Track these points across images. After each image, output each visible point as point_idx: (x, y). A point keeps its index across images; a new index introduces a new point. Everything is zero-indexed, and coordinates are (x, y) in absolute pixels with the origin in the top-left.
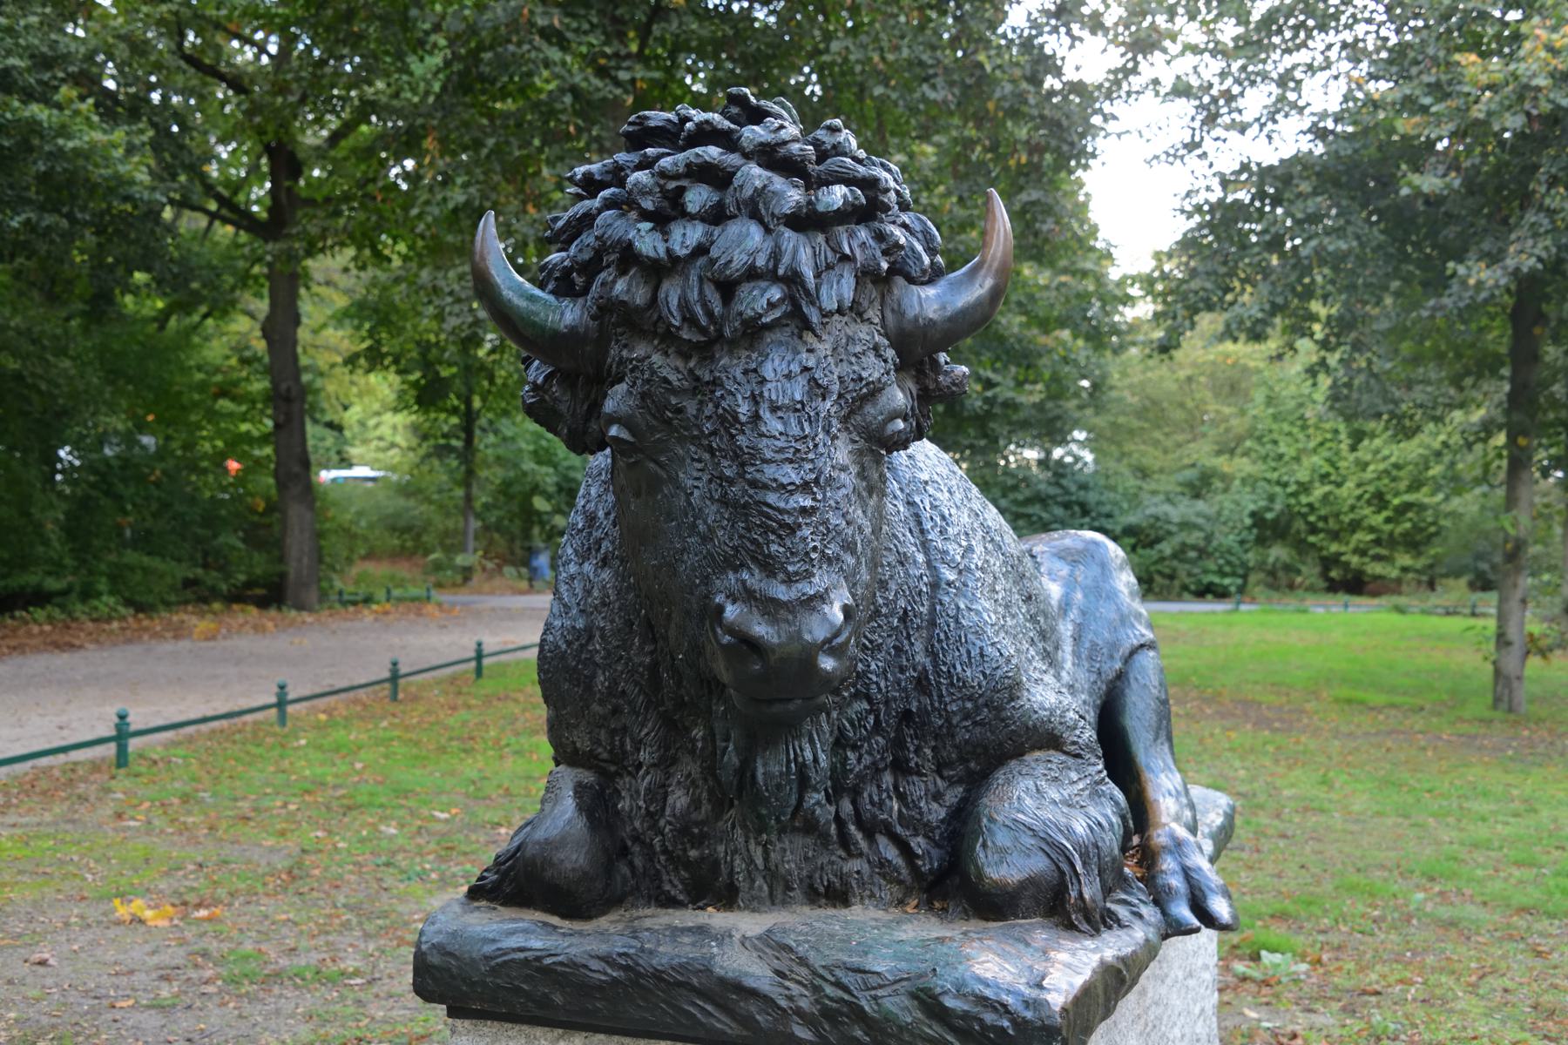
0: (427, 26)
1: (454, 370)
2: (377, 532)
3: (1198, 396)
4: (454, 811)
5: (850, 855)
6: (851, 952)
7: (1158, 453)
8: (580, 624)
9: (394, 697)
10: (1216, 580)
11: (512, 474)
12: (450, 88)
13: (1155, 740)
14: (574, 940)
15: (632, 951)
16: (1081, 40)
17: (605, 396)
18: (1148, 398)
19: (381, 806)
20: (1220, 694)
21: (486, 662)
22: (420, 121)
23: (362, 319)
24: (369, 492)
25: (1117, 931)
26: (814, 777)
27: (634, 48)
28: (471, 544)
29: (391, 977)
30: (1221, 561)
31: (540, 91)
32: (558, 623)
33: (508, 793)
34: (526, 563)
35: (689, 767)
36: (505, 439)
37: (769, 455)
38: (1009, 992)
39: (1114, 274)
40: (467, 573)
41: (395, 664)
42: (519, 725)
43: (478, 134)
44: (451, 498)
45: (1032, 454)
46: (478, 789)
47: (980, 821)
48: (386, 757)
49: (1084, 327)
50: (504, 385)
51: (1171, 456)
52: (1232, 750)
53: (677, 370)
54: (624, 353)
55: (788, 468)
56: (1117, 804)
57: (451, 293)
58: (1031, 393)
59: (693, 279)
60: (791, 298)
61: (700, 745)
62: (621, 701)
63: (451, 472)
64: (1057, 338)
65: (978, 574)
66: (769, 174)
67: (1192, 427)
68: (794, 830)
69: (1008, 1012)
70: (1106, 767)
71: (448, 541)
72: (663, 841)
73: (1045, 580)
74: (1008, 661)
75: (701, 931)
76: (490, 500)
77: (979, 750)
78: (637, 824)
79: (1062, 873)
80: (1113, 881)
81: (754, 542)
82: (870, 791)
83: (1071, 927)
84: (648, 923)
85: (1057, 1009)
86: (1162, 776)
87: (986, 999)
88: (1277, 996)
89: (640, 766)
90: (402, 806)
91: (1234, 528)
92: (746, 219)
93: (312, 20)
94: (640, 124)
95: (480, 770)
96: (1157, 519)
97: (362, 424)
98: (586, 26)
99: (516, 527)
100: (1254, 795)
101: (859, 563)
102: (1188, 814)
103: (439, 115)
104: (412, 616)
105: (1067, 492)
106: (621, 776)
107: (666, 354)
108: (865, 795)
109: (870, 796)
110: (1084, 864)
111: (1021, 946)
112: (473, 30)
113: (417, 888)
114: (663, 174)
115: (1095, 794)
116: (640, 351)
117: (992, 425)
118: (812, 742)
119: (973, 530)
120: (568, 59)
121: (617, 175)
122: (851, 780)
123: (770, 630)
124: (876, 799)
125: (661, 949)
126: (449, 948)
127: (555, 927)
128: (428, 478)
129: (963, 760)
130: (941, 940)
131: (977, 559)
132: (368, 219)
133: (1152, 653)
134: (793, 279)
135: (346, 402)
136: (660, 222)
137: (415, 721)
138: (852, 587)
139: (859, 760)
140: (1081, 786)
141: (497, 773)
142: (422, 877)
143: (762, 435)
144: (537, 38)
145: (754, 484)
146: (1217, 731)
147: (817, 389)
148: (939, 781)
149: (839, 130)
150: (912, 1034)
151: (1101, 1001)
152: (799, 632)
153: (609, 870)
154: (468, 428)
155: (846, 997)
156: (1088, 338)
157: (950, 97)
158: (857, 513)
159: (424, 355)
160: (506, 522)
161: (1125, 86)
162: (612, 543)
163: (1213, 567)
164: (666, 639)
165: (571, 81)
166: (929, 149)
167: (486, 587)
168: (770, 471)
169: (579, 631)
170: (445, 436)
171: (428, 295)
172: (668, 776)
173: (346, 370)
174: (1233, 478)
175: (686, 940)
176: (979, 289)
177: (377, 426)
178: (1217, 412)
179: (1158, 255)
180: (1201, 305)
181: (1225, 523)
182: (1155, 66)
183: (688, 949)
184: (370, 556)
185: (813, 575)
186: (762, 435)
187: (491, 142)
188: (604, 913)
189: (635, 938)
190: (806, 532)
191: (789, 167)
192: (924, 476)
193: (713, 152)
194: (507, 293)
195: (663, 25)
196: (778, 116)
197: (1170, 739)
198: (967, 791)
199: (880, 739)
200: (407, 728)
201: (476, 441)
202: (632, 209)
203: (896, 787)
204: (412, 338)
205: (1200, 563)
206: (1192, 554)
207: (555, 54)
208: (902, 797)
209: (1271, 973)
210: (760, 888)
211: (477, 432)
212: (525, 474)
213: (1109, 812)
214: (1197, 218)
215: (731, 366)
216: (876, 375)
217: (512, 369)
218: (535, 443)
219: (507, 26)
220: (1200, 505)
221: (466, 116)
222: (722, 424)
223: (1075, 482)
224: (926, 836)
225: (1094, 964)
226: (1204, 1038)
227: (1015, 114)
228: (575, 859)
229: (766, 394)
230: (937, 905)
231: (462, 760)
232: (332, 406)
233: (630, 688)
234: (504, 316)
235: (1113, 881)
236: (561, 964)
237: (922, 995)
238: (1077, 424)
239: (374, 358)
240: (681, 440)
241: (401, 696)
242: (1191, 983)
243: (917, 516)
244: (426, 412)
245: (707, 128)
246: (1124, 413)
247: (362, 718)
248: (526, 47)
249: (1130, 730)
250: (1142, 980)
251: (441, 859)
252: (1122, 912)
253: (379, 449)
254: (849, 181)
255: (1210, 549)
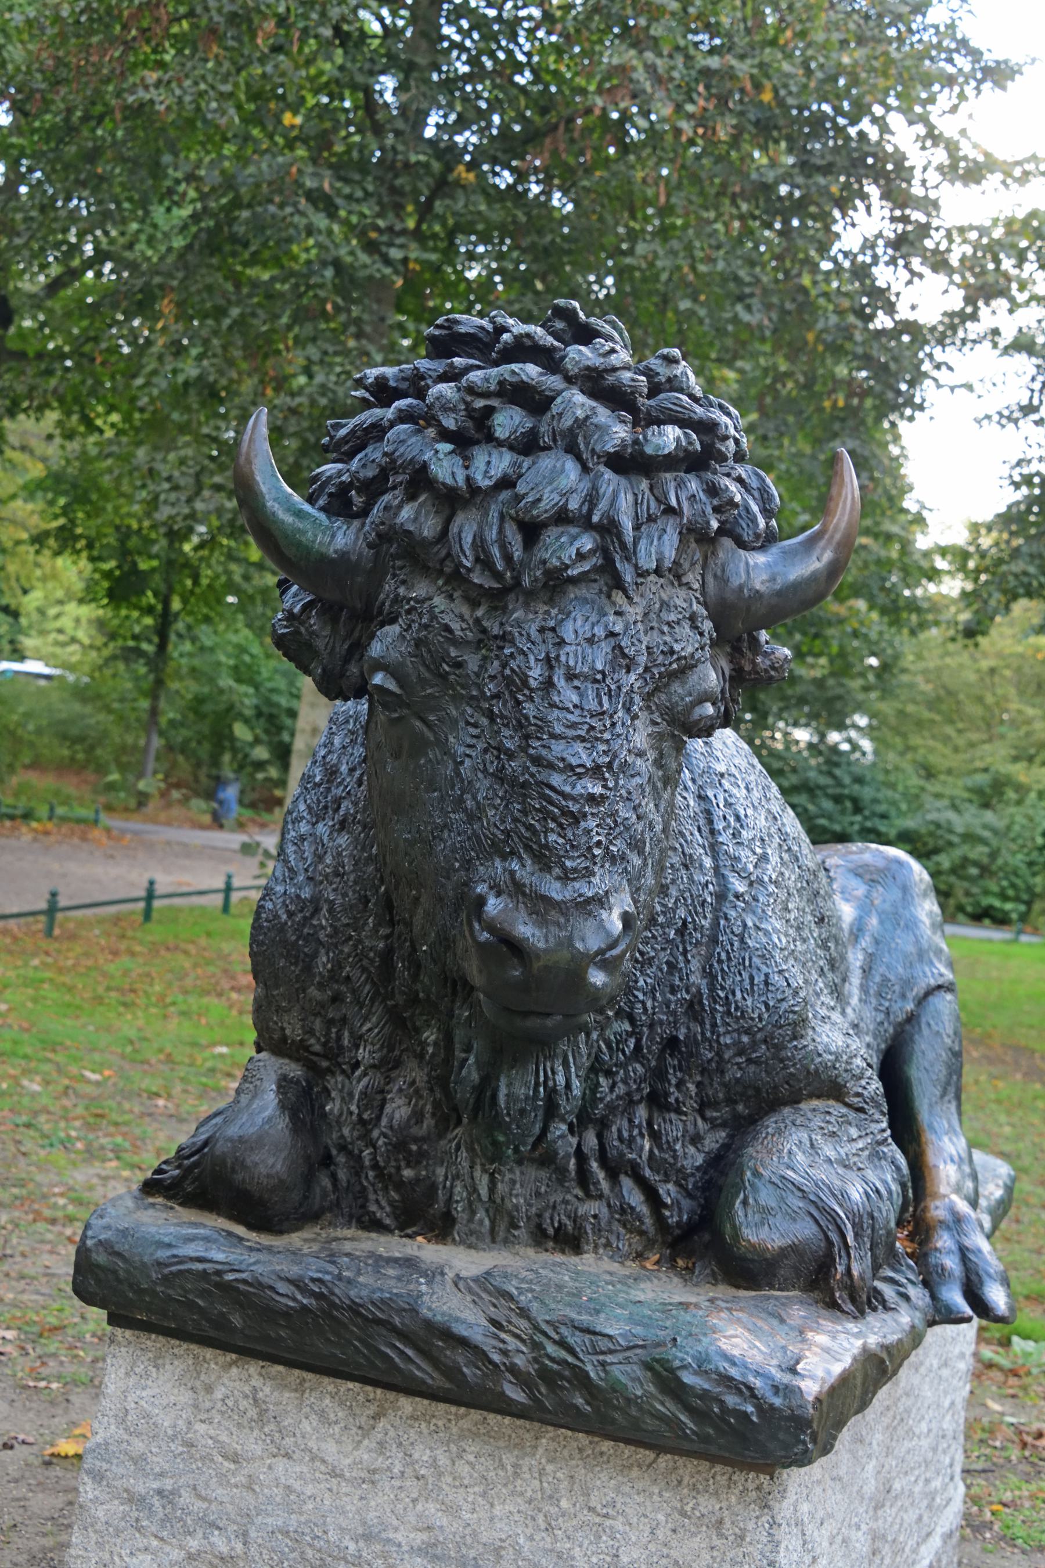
0: (179, 175)
1: (155, 563)
2: (46, 740)
3: (1000, 691)
4: (107, 1073)
5: (588, 1195)
6: (580, 1308)
7: (947, 751)
8: (306, 893)
9: (49, 932)
10: (997, 903)
11: (206, 690)
12: (197, 247)
13: (942, 1096)
14: (262, 1256)
15: (328, 1277)
16: (921, 276)
17: (372, 636)
18: (944, 687)
19: (25, 1057)
20: (989, 1036)
21: (157, 904)
22: (157, 280)
23: (58, 493)
24: (41, 691)
25: (881, 1314)
26: (564, 1105)
27: (411, 224)
28: (151, 765)
29: (23, 1255)
30: (1005, 883)
31: (295, 258)
32: (279, 889)
33: (169, 1059)
34: (210, 795)
35: (414, 1073)
36: (202, 649)
37: (558, 729)
38: (757, 1374)
39: (922, 542)
40: (142, 799)
41: (54, 895)
42: (189, 982)
43: (222, 302)
44: (134, 709)
45: (803, 735)
46: (136, 1051)
47: (742, 1174)
48: (35, 1000)
49: (882, 599)
50: (209, 586)
51: (962, 756)
52: (998, 1102)
53: (461, 617)
54: (402, 591)
55: (579, 747)
56: (898, 1169)
57: (169, 479)
58: (813, 666)
59: (494, 515)
60: (604, 551)
61: (430, 1050)
62: (343, 988)
63: (137, 679)
64: (850, 608)
65: (772, 888)
66: (594, 404)
67: (989, 726)
68: (532, 1160)
69: (754, 1396)
70: (891, 1125)
71: (124, 759)
72: (374, 1155)
73: (837, 897)
74: (796, 993)
75: (409, 1263)
76: (179, 717)
77: (750, 1092)
78: (346, 1131)
79: (830, 1243)
80: (884, 1256)
81: (529, 827)
82: (620, 1123)
83: (833, 1305)
84: (348, 1246)
85: (811, 1399)
86: (946, 1139)
87: (731, 1379)
88: (1025, 1388)
89: (357, 1065)
90: (49, 1060)
91: (1023, 846)
92: (561, 453)
93: (51, 155)
94: (449, 328)
95: (140, 1029)
96: (938, 826)
97: (42, 612)
98: (359, 194)
99: (204, 751)
100: (1019, 1157)
101: (645, 864)
102: (969, 1185)
103: (180, 275)
104: (76, 840)
105: (839, 784)
106: (333, 1074)
107: (451, 598)
108: (614, 1129)
109: (619, 1131)
110: (856, 1235)
111: (775, 1322)
112: (229, 183)
113: (60, 1157)
114: (471, 390)
115: (876, 1156)
116: (421, 589)
117: (762, 696)
118: (566, 1064)
119: (770, 835)
120: (336, 228)
121: (416, 384)
122: (600, 1110)
123: (537, 933)
124: (626, 1134)
125: (361, 1279)
126: (118, 1248)
127: (241, 1239)
128: (110, 683)
129: (731, 1101)
130: (685, 1306)
131: (771, 871)
132: (83, 382)
133: (949, 997)
134: (609, 528)
135: (27, 586)
136: (462, 442)
137: (70, 962)
138: (635, 892)
139: (612, 1088)
140: (860, 1144)
141: (159, 1035)
142: (66, 1145)
143: (553, 705)
144: (303, 201)
145: (537, 761)
146: (983, 1078)
147: (622, 659)
148: (700, 1121)
149: (677, 362)
150: (641, 1409)
151: (858, 1393)
152: (570, 939)
153: (308, 1180)
154: (162, 631)
155: (570, 1359)
156: (884, 611)
157: (766, 322)
158: (649, 807)
159: (123, 542)
160: (193, 744)
161: (961, 334)
162: (355, 804)
163: (995, 889)
164: (409, 924)
165: (334, 253)
166: (731, 375)
167: (163, 816)
168: (558, 748)
169: (304, 901)
170: (135, 637)
171: (143, 478)
172: (389, 1080)
173: (32, 550)
174: (1028, 790)
175: (391, 1272)
176: (816, 563)
177: (58, 616)
178: (1019, 712)
179: (975, 528)
180: (1021, 591)
181: (1014, 840)
182: (994, 315)
183: (393, 1282)
184: (35, 765)
185: (593, 874)
186: (553, 705)
187: (235, 312)
188: (297, 1229)
189: (333, 1263)
190: (592, 823)
191: (617, 399)
192: (721, 768)
193: (531, 371)
194: (271, 505)
195: (448, 202)
196: (609, 338)
197: (958, 1098)
198: (731, 1136)
199: (638, 1066)
200: (61, 970)
201: (170, 647)
202: (429, 425)
203: (650, 1124)
204: (112, 522)
205: (982, 882)
206: (974, 871)
207: (321, 221)
208: (655, 1136)
209: (1020, 1361)
210: (481, 1222)
211: (173, 637)
212: (221, 691)
213: (889, 1178)
214: (1024, 490)
215: (526, 620)
216: (690, 650)
217: (220, 569)
218: (237, 657)
219: (270, 184)
220: (989, 816)
221: (209, 280)
222: (507, 686)
223: (850, 773)
224: (678, 1184)
225: (855, 1351)
226: (950, 1434)
227: (837, 350)
228: (271, 1165)
229: (563, 658)
230: (681, 1263)
231: (120, 1014)
232: (11, 588)
233: (355, 974)
234: (266, 531)
235: (884, 1256)
236: (245, 1281)
237: (657, 1367)
238: (860, 707)
239: (66, 540)
240: (456, 699)
241: (57, 932)
242: (945, 1372)
243: (708, 813)
244: (117, 608)
245: (527, 342)
246: (914, 702)
247: (10, 952)
248: (289, 210)
249: (914, 1082)
250: (903, 1372)
251: (89, 1127)
252: (888, 1291)
253: (57, 643)
254: (683, 423)
255: (994, 868)
